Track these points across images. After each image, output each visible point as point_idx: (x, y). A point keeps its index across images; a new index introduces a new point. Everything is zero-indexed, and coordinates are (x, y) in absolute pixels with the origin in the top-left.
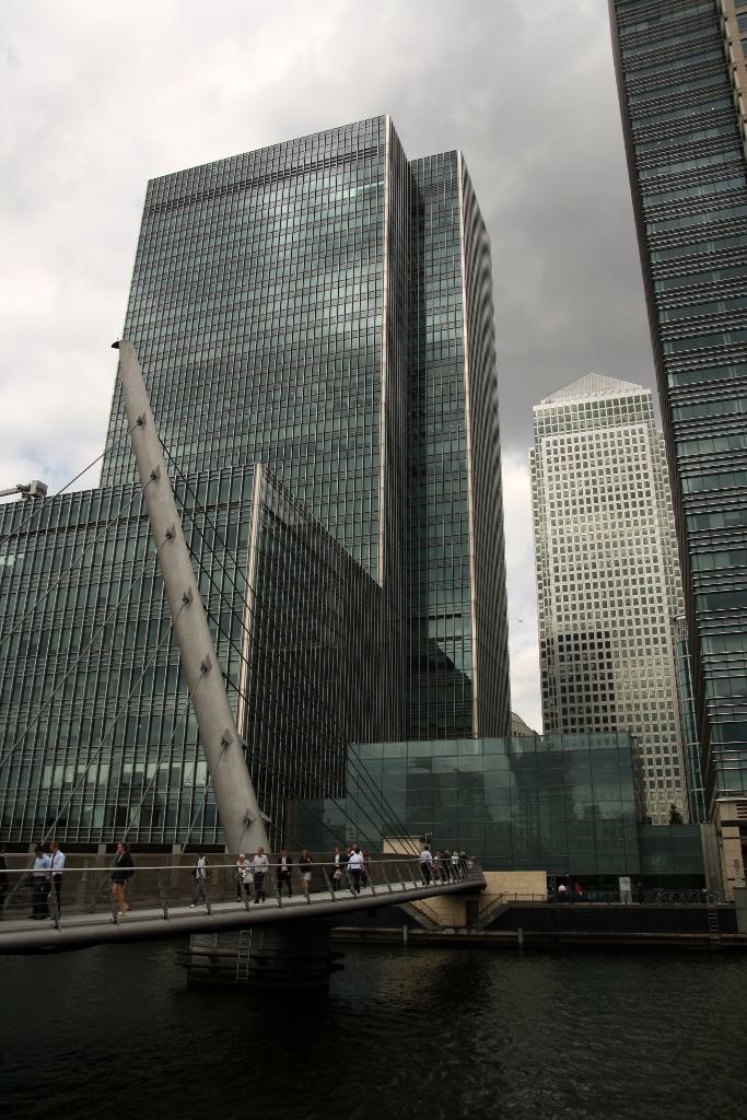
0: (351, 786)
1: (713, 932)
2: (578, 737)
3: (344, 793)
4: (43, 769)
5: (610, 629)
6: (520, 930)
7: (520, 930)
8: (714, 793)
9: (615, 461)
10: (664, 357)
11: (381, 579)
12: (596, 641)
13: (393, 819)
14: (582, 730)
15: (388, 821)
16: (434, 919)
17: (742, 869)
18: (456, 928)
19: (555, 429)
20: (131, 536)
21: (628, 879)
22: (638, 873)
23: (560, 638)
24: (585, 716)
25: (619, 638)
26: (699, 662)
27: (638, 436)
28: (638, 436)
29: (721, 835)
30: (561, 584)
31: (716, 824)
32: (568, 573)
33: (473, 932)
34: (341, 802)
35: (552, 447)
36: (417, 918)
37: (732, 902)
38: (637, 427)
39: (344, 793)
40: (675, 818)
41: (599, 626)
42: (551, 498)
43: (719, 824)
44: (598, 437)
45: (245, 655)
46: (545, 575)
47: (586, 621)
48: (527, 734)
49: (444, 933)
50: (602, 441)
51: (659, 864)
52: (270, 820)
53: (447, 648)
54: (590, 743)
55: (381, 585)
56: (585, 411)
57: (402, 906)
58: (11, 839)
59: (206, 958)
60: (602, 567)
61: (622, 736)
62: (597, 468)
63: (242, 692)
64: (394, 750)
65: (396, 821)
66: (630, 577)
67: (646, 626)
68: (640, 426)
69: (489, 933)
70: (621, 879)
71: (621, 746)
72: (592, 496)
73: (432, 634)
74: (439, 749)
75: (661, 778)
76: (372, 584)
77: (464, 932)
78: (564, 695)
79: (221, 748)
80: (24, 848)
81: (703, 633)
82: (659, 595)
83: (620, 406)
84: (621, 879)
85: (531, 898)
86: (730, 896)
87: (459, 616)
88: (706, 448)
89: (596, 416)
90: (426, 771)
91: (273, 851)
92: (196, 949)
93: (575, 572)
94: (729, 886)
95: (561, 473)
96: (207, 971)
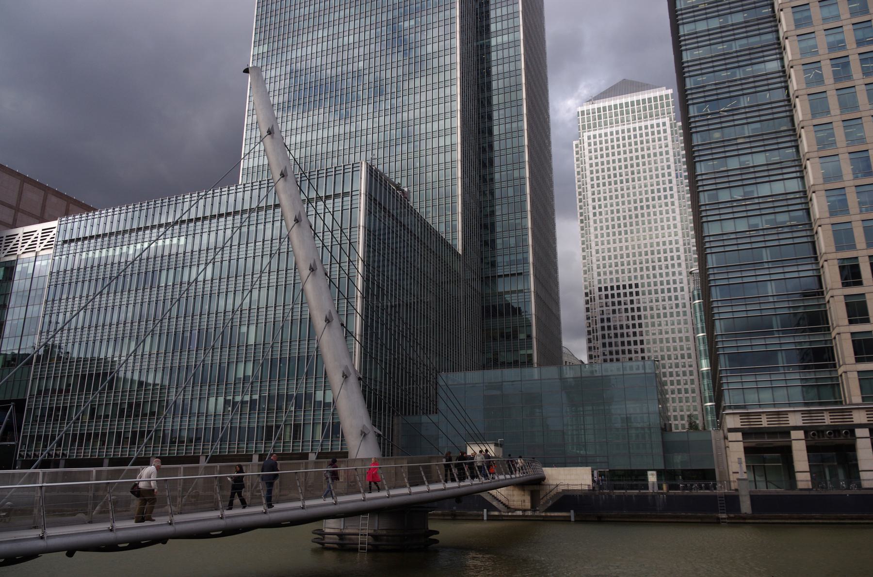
0: (442, 406)
1: (721, 513)
2: (615, 365)
3: (436, 411)
4: (208, 400)
6: (572, 511)
7: (572, 511)
8: (722, 407)
10: (686, 91)
11: (460, 248)
13: (474, 428)
14: (618, 360)
15: (471, 432)
16: (507, 503)
17: (744, 465)
18: (524, 510)
21: (655, 473)
22: (663, 467)
26: (706, 273)
29: (727, 439)
31: (723, 430)
33: (537, 513)
34: (434, 418)
36: (495, 503)
37: (736, 490)
38: (661, 121)
39: (436, 411)
40: (693, 426)
41: (630, 279)
42: (598, 268)
43: (726, 431)
45: (360, 270)
46: (584, 192)
47: (620, 275)
48: (576, 362)
49: (514, 514)
51: (679, 461)
52: (381, 433)
53: (514, 300)
54: (624, 369)
55: (460, 252)
57: (482, 494)
59: (335, 536)
61: (648, 363)
63: (357, 339)
64: (474, 377)
65: (476, 432)
68: (664, 120)
69: (549, 514)
70: (649, 473)
71: (648, 371)
73: (500, 289)
74: (510, 374)
75: (681, 395)
77: (529, 513)
79: (342, 379)
80: (196, 460)
81: (716, 317)
82: (678, 253)
84: (649, 473)
85: (579, 488)
86: (734, 486)
88: (729, 226)
90: (498, 393)
91: (384, 455)
92: (327, 531)
94: (733, 477)
96: (336, 546)
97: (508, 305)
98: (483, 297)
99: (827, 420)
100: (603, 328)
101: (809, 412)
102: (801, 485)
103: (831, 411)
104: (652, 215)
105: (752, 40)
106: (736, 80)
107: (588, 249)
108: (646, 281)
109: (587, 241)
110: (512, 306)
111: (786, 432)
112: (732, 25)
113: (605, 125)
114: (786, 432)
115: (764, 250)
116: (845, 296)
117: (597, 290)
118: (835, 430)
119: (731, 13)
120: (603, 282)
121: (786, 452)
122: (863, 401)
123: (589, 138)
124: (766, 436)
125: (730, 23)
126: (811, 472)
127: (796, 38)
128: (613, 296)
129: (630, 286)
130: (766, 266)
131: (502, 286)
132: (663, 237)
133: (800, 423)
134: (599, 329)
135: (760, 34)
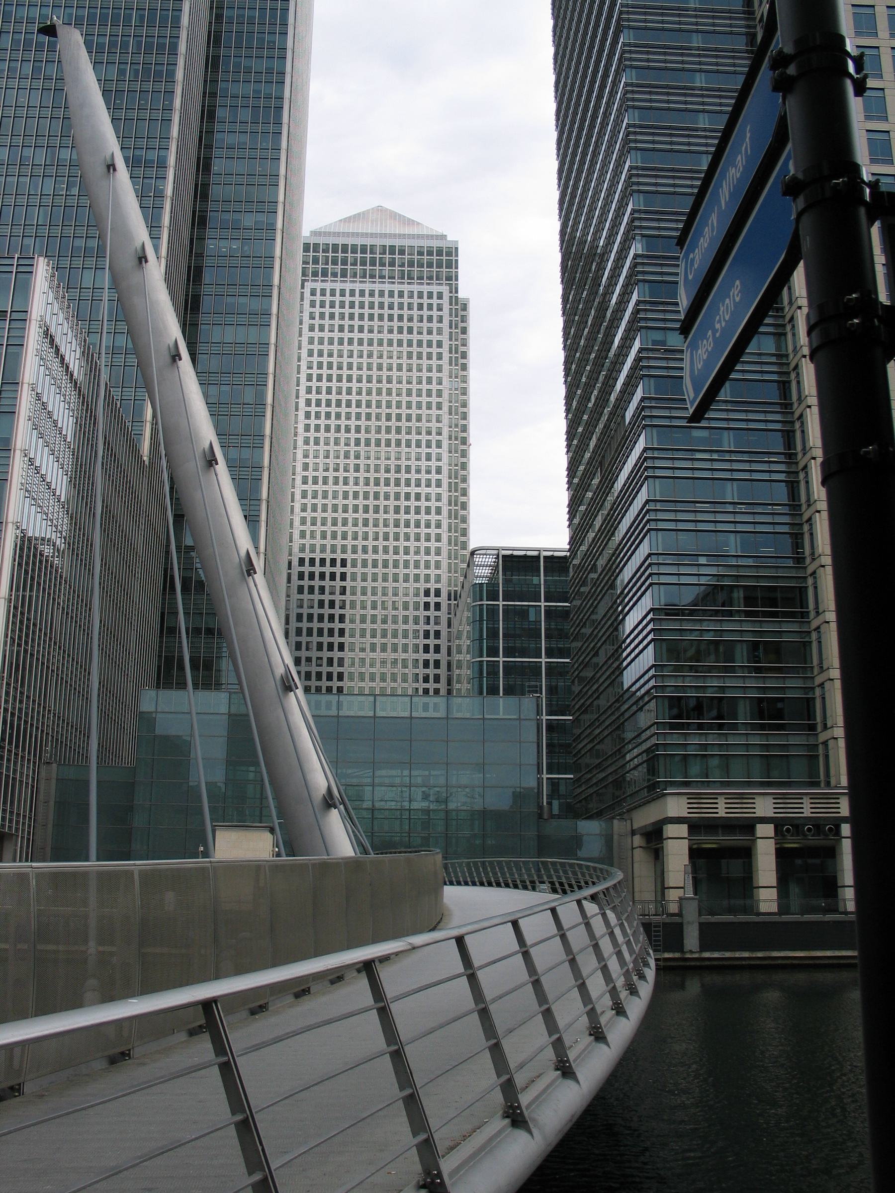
19: (325, 273)
23: (302, 561)
24: (325, 669)
25: (359, 570)
27: (435, 301)
28: (435, 301)
32: (321, 474)
35: (318, 298)
38: (435, 289)
50: (386, 300)
60: (316, 470)
62: (425, 337)
66: (404, 489)
72: (335, 372)
78: (302, 569)
83: (340, 255)
89: (382, 264)
93: (331, 474)
95: (326, 335)
99: (807, 810)
102: (764, 908)
111: (748, 826)
114: (748, 826)
118: (817, 825)
121: (746, 854)
123: (313, 293)
124: (720, 832)
128: (312, 576)
129: (333, 562)
133: (770, 813)
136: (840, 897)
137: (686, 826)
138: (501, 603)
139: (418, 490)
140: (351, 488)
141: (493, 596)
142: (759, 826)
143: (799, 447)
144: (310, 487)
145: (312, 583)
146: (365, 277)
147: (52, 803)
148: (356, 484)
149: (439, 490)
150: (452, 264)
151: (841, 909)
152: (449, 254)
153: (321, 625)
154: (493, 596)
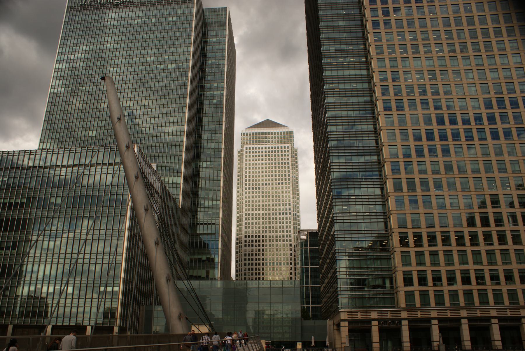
5: (264, 234)
9: (282, 159)
12: (258, 239)
20: (16, 176)
21: (301, 343)
27: (286, 149)
28: (286, 149)
30: (247, 267)
35: (248, 150)
38: (286, 145)
44: (285, 148)
46: (241, 179)
55: (180, 207)
56: (264, 136)
58: (4, 323)
67: (287, 234)
68: (288, 145)
70: (298, 343)
76: (177, 206)
84: (298, 343)
87: (214, 224)
97: (201, 242)
98: (190, 236)
99: (389, 316)
100: (245, 260)
101: (351, 312)
103: (391, 311)
104: (278, 197)
105: (337, 112)
106: (353, 132)
107: (240, 212)
108: (268, 234)
109: (240, 208)
110: (204, 242)
111: (369, 321)
112: (352, 103)
113: (268, 142)
114: (369, 321)
115: (363, 223)
116: (401, 252)
117: (244, 237)
118: (393, 321)
119: (352, 96)
120: (247, 233)
121: (369, 331)
122: (406, 306)
123: (246, 149)
125: (351, 101)
126: (410, 342)
127: (384, 115)
130: (363, 232)
131: (201, 230)
132: (283, 210)
134: (243, 260)
135: (335, 111)
136: (462, 345)
137: (377, 322)
138: (309, 248)
139: (273, 212)
140: (261, 212)
141: (306, 245)
142: (372, 322)
143: (385, 192)
144: (288, 212)
145: (253, 243)
146: (263, 143)
147: (144, 318)
148: (263, 210)
149: (290, 211)
150: (292, 137)
151: (493, 348)
152: (290, 134)
153: (253, 257)
154: (306, 245)
